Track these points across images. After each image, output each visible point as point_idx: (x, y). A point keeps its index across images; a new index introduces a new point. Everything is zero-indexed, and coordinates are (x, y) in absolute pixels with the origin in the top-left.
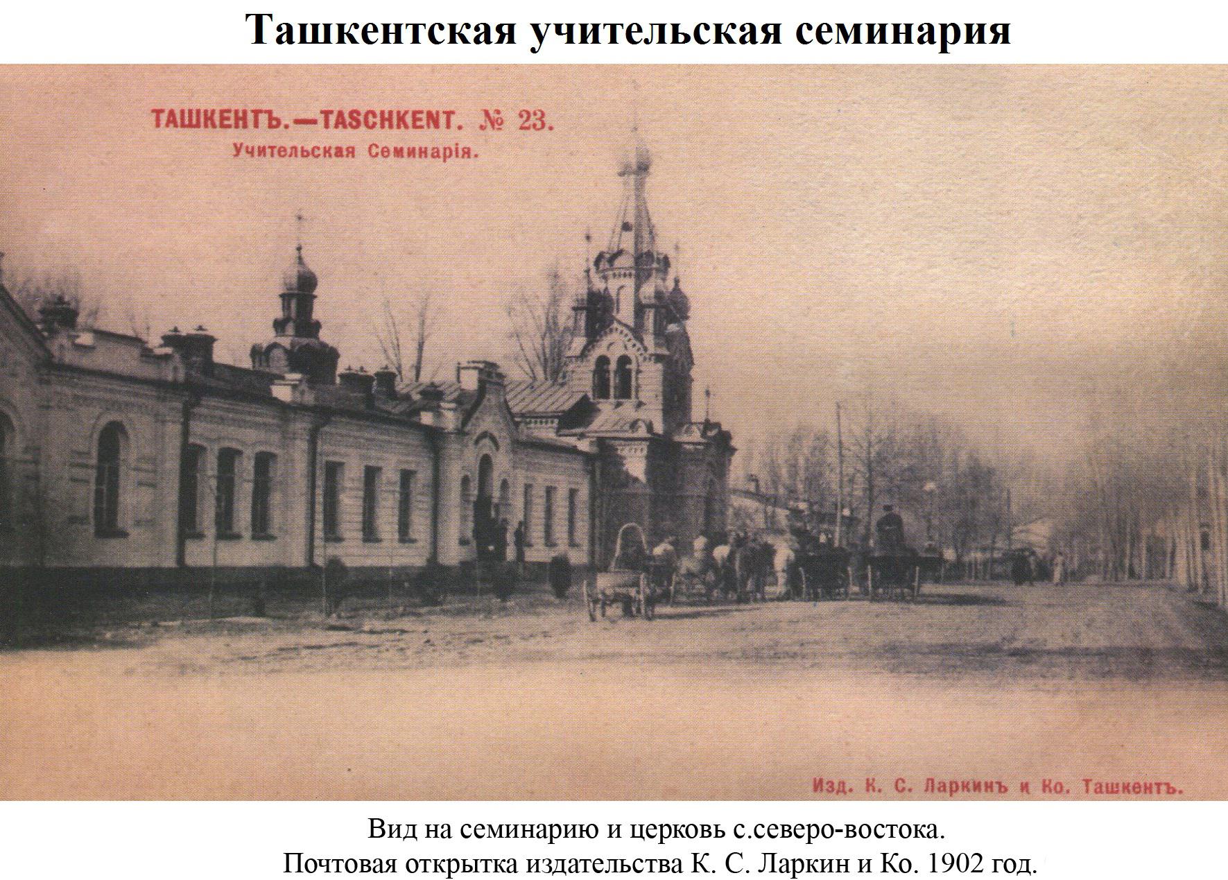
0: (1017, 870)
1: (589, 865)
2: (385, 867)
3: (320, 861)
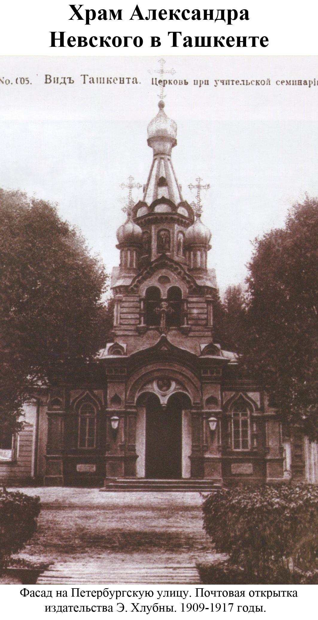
0: (249, 610)
1: (72, 608)
2: (240, 594)
3: (212, 592)
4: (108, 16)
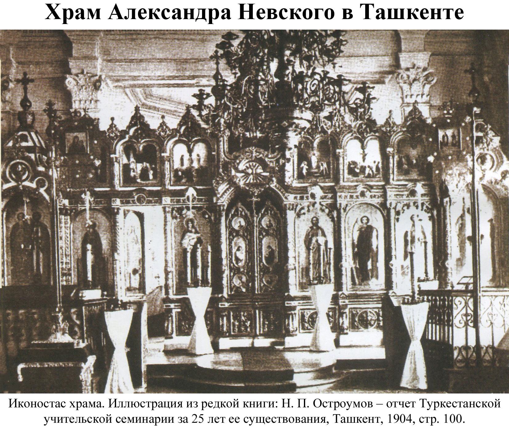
1: (68, 420)
4: (88, 405)
